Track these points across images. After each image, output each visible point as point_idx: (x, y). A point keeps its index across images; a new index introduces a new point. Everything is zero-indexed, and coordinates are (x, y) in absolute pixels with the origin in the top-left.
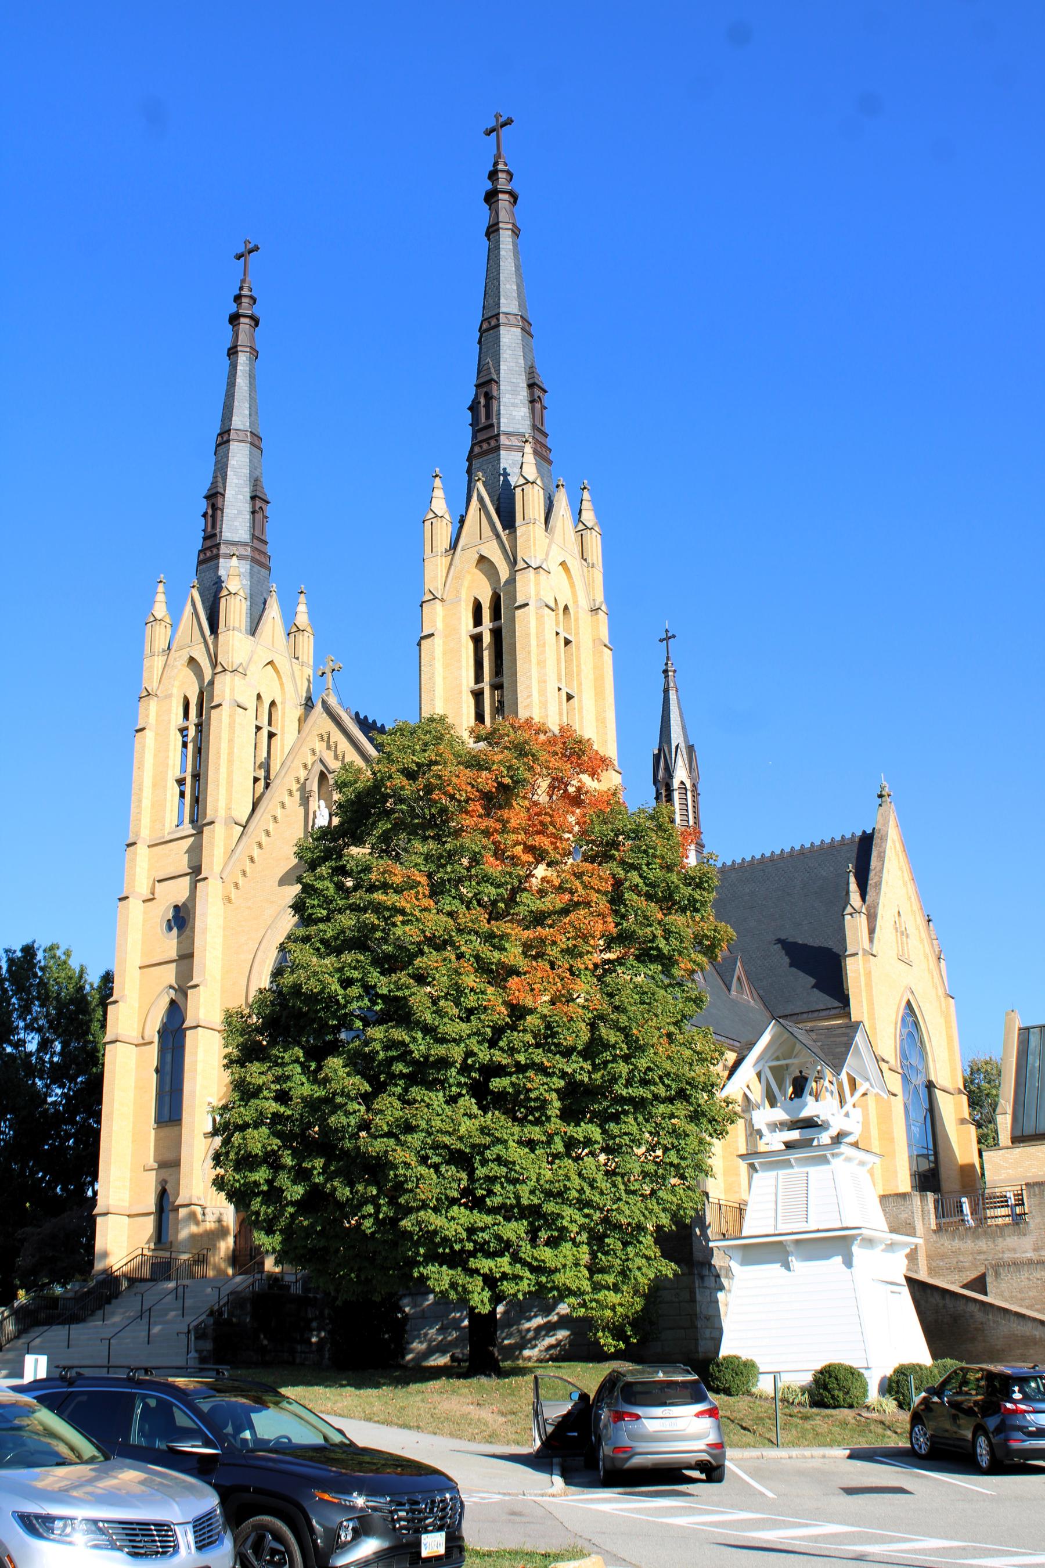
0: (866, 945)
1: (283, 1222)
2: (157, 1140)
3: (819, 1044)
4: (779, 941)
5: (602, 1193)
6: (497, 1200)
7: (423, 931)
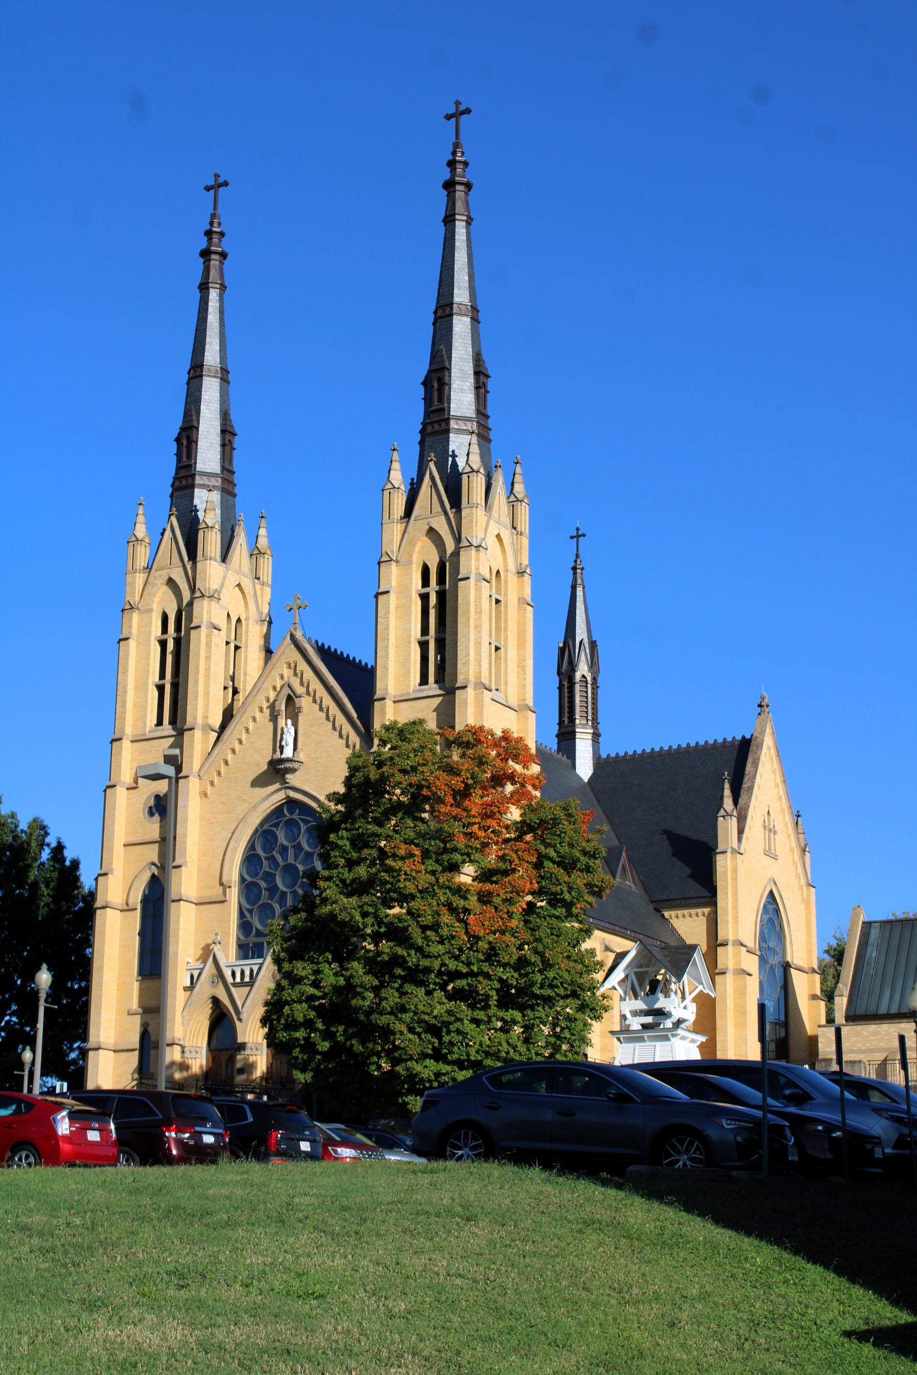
0: (735, 844)
1: (313, 1065)
2: (141, 990)
3: (669, 959)
4: (665, 832)
5: (520, 1055)
6: (455, 1056)
7: (417, 886)
